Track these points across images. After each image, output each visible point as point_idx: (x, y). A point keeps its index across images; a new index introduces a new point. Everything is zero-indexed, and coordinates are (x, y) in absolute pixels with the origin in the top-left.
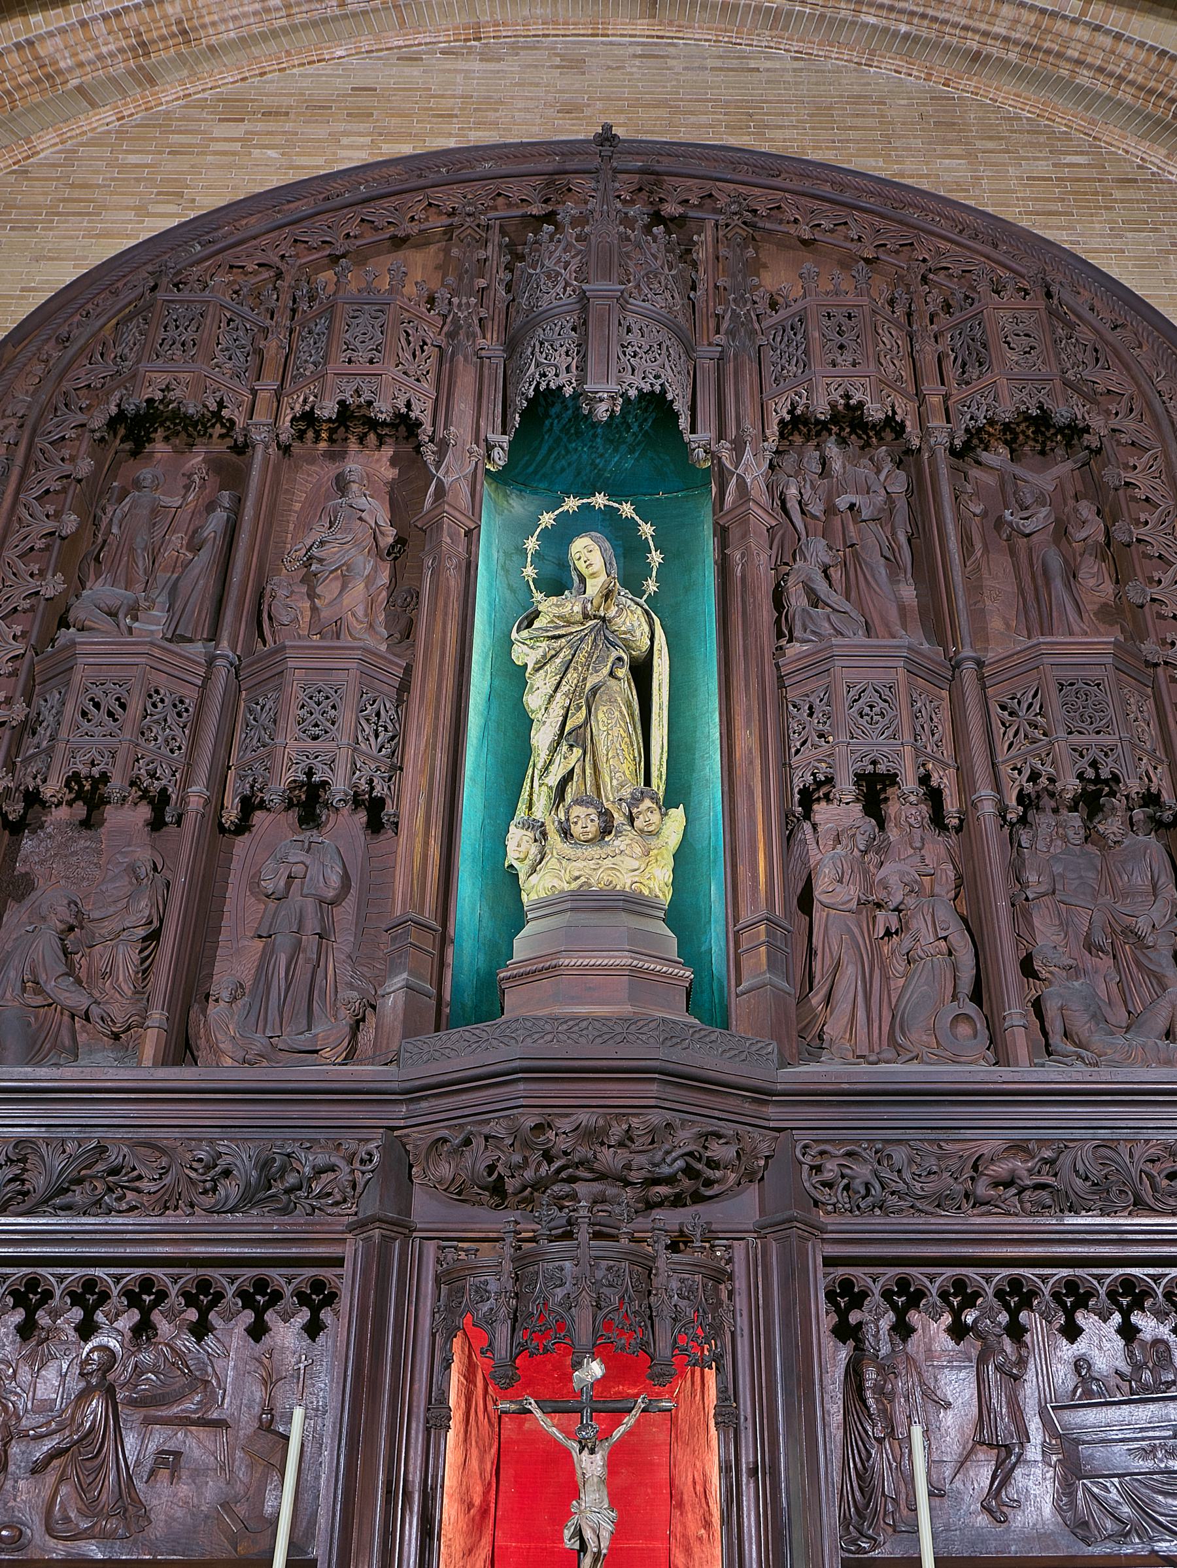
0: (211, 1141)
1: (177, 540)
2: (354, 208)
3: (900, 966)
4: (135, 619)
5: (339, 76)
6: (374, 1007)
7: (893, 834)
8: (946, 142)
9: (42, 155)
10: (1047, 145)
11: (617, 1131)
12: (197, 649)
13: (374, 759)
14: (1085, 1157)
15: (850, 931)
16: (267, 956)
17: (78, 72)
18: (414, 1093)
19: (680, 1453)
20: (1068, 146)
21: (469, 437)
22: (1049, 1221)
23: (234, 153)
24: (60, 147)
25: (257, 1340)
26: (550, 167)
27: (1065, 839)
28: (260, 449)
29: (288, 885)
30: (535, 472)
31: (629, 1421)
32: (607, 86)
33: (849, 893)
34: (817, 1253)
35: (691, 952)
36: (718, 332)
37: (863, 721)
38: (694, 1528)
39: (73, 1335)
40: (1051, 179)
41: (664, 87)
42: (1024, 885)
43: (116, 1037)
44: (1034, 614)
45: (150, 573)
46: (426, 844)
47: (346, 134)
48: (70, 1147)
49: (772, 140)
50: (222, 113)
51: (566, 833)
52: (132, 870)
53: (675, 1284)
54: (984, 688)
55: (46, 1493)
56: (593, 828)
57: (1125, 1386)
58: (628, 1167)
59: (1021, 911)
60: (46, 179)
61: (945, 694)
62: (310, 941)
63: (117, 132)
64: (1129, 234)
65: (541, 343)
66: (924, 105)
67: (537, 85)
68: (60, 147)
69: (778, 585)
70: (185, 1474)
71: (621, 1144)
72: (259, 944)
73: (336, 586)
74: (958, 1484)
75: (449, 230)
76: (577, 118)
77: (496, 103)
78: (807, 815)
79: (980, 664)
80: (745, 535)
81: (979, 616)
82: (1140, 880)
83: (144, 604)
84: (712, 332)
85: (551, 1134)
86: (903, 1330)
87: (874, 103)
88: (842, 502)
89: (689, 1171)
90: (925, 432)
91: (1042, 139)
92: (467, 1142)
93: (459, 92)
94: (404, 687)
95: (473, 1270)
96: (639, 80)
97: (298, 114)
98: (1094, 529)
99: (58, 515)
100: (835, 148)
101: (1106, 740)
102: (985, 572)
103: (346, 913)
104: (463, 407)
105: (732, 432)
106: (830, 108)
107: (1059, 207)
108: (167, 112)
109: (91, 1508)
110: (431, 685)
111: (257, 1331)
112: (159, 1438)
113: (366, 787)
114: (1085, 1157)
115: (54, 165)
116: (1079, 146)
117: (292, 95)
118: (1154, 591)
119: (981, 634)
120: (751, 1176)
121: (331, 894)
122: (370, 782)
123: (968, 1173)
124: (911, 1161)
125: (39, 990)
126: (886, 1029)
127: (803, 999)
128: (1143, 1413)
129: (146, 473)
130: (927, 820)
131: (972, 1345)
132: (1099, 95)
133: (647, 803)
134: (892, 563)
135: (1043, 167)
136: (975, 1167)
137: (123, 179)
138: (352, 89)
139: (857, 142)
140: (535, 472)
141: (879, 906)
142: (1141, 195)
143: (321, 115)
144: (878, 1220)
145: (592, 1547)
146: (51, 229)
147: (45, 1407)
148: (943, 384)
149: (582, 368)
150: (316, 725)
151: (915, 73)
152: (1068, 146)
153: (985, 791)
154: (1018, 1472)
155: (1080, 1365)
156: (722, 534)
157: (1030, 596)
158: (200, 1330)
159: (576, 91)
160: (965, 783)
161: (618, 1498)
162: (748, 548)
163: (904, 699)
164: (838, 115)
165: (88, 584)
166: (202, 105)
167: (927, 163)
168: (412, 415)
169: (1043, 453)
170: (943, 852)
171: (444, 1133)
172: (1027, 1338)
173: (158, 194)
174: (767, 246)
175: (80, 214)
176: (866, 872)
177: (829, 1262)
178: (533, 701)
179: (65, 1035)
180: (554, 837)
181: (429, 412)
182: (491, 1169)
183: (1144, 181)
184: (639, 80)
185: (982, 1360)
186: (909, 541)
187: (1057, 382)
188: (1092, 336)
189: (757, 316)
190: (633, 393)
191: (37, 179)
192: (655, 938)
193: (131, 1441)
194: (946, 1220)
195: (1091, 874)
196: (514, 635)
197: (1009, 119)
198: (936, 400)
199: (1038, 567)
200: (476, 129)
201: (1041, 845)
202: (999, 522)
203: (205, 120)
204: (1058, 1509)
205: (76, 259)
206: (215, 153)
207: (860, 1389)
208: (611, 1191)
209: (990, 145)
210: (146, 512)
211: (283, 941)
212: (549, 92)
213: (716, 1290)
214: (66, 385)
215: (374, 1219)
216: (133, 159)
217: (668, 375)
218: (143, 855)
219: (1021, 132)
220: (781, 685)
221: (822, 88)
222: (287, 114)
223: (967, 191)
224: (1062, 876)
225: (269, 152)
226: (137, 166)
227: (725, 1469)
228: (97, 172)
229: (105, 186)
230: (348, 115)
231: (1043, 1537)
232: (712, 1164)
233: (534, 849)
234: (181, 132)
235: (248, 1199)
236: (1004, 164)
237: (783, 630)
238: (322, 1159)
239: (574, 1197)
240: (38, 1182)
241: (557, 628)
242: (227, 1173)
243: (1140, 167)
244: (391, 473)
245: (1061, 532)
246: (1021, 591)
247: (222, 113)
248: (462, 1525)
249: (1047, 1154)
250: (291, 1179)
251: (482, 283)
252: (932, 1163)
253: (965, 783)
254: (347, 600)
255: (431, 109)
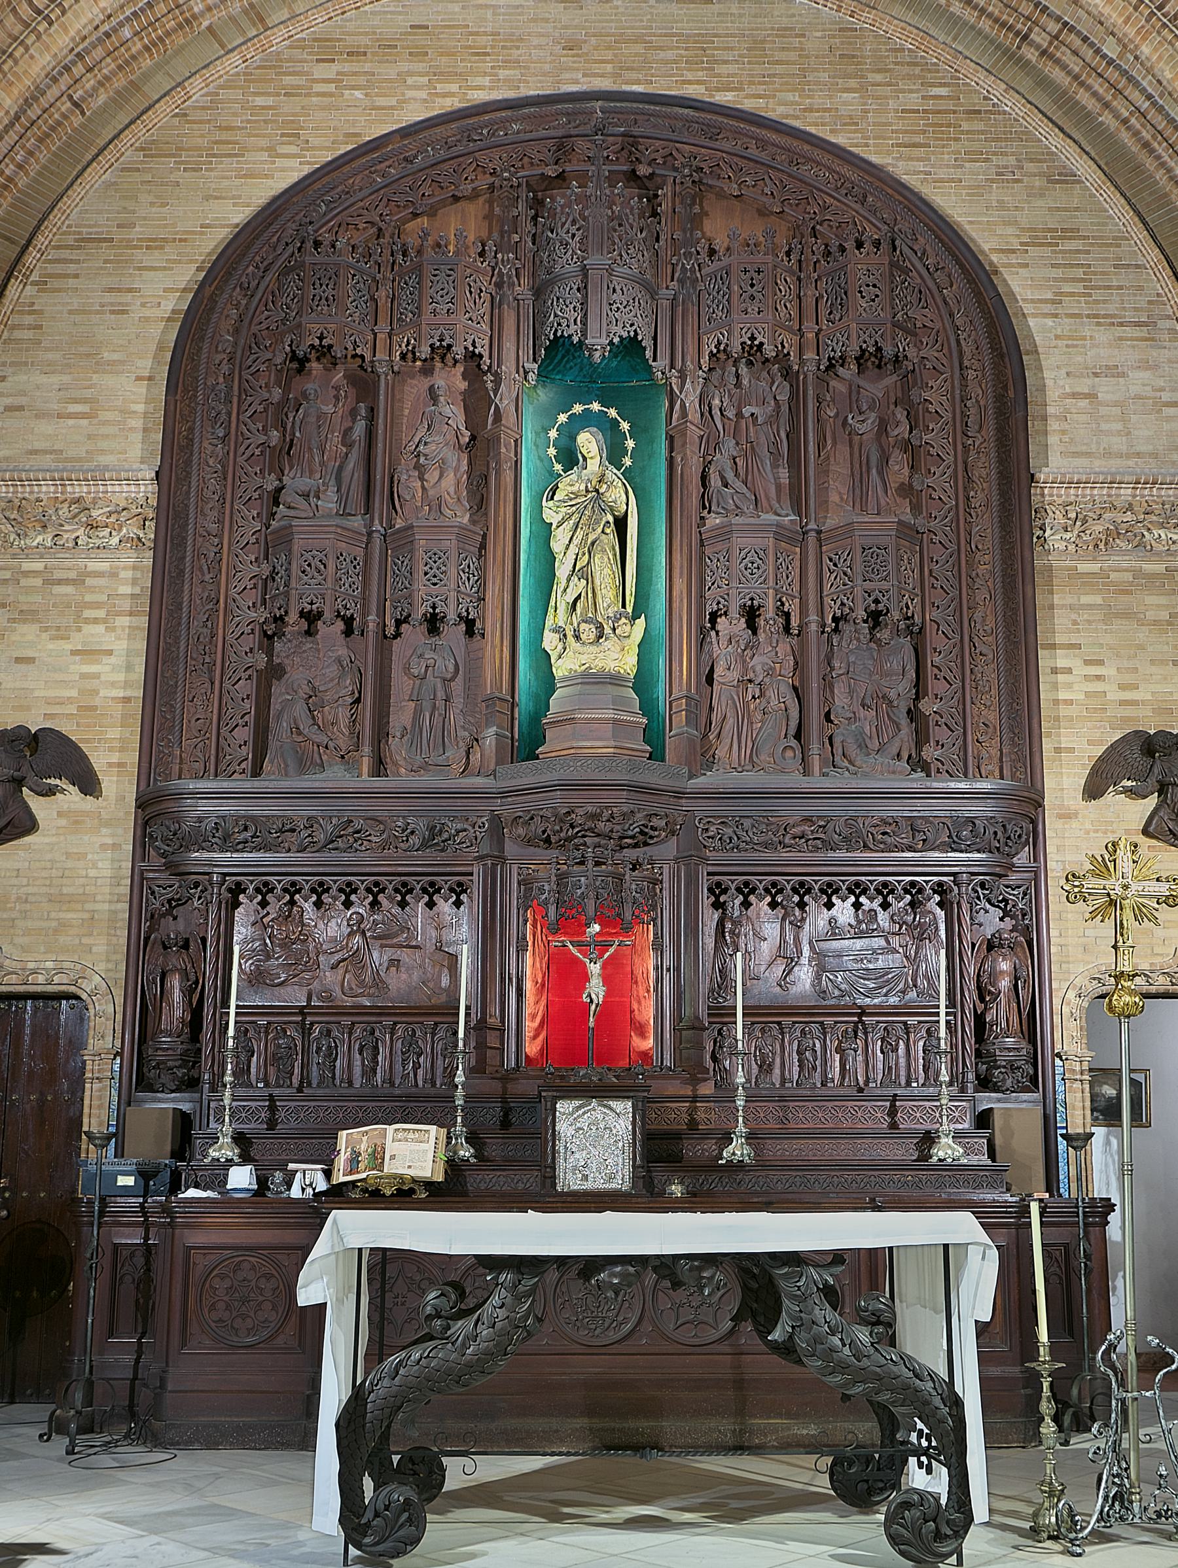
0: (404, 817)
1: (336, 437)
2: (427, 171)
3: (759, 716)
4: (318, 498)
5: (400, 13)
6: (477, 740)
7: (762, 636)
8: (847, 76)
9: (194, 98)
10: (920, 77)
11: (606, 814)
12: (357, 523)
13: (469, 595)
14: (840, 825)
15: (733, 698)
16: (418, 713)
17: (208, 15)
18: (504, 794)
19: (636, 960)
20: (936, 78)
21: (513, 370)
22: (820, 855)
23: (331, 95)
24: (206, 90)
25: (431, 909)
26: (560, 133)
27: (858, 640)
28: (383, 377)
29: (426, 671)
30: (553, 369)
31: (612, 950)
32: (600, 21)
33: (734, 675)
34: (703, 871)
35: (648, 707)
36: (672, 280)
37: (747, 573)
38: (642, 992)
39: (342, 907)
40: (918, 111)
41: (642, 21)
42: (832, 669)
43: (343, 757)
44: (858, 491)
45: (323, 464)
46: (502, 650)
47: (411, 74)
48: (334, 821)
49: (719, 75)
50: (318, 53)
51: (577, 637)
52: (339, 661)
53: (634, 887)
54: (821, 546)
55: (340, 978)
56: (592, 636)
57: (852, 931)
58: (612, 831)
59: (828, 683)
60: (201, 122)
61: (798, 550)
62: (440, 704)
63: (245, 74)
64: (967, 165)
65: (558, 299)
66: (834, 37)
67: (547, 20)
68: (206, 90)
69: (704, 470)
70: (403, 969)
71: (608, 820)
72: (412, 704)
73: (437, 474)
74: (767, 974)
75: (492, 187)
76: (578, 55)
77: (517, 40)
78: (713, 628)
79: (819, 532)
80: (685, 444)
81: (823, 490)
82: (896, 665)
83: (322, 488)
84: (669, 279)
85: (573, 816)
86: (746, 904)
87: (797, 36)
88: (747, 411)
89: (642, 833)
90: (802, 362)
91: (917, 70)
92: (532, 818)
93: (489, 29)
94: (483, 546)
95: (537, 880)
96: (623, 14)
97: (374, 54)
98: (903, 430)
99: (265, 430)
100: (765, 83)
101: (885, 585)
102: (832, 459)
103: (457, 686)
104: (509, 345)
105: (679, 364)
106: (763, 42)
107: (920, 139)
108: (278, 53)
109: (362, 984)
110: (499, 553)
111: (431, 905)
112: (389, 953)
113: (465, 614)
114: (840, 825)
115: (203, 108)
116: (943, 78)
117: (367, 34)
118: (929, 481)
119: (824, 504)
120: (673, 833)
121: (449, 676)
122: (467, 611)
123: (782, 832)
124: (753, 826)
125: (300, 733)
126: (748, 752)
127: (705, 736)
128: (859, 944)
129: (310, 387)
130: (781, 629)
131: (780, 912)
132: (966, 23)
133: (623, 620)
134: (775, 455)
135: (913, 100)
136: (785, 829)
137: (256, 121)
138: (412, 27)
139: (781, 76)
140: (553, 369)
141: (750, 681)
142: (980, 126)
143: (390, 54)
144: (735, 854)
145: (596, 1001)
146: (211, 170)
147: (334, 940)
148: (817, 324)
149: (584, 323)
150: (435, 576)
151: (829, 5)
152: (936, 78)
153: (813, 617)
154: (796, 969)
155: (832, 921)
156: (671, 439)
157: (857, 479)
158: (403, 904)
159: (576, 27)
160: (803, 612)
161: (607, 979)
162: (685, 454)
163: (771, 558)
164: (770, 49)
165: (286, 472)
166: (300, 45)
167: (831, 97)
168: (477, 351)
169: (879, 367)
170: (789, 648)
171: (520, 814)
172: (807, 908)
173: (283, 135)
174: (710, 195)
175: (230, 155)
176: (745, 661)
177: (709, 874)
178: (557, 546)
179: (316, 756)
180: (571, 639)
181: (487, 347)
182: (544, 832)
183: (986, 112)
184: (623, 14)
185: (783, 919)
186: (787, 436)
187: (889, 325)
188: (919, 281)
189: (699, 265)
190: (616, 340)
191: (194, 122)
192: (626, 700)
193: (375, 955)
194: (769, 855)
195: (871, 662)
196: (544, 503)
197: (897, 50)
198: (811, 335)
199: (864, 458)
200: (505, 68)
201: (844, 644)
202: (845, 423)
203: (305, 61)
204: (813, 986)
205: (233, 197)
206: (319, 94)
207: (723, 932)
208: (603, 842)
209: (878, 77)
210: (314, 420)
211: (427, 705)
212: (555, 27)
213: (654, 888)
214: (254, 329)
215: (487, 856)
216: (260, 101)
217: (639, 321)
218: (343, 652)
219: (902, 64)
220: (702, 545)
221: (759, 20)
222: (365, 54)
223: (857, 124)
224: (854, 663)
225: (356, 93)
226: (263, 108)
227: (656, 968)
228: (235, 114)
229: (243, 128)
230: (411, 54)
231: (803, 996)
232: (653, 829)
233: (560, 646)
234: (290, 74)
235: (424, 845)
236: (886, 98)
237: (705, 504)
238: (459, 826)
239: (585, 844)
240: (321, 837)
241: (571, 499)
242: (412, 833)
243: (985, 98)
244: (463, 385)
245: (883, 427)
246: (852, 474)
247: (318, 53)
248: (534, 991)
249: (822, 823)
250: (445, 836)
251: (516, 237)
252: (763, 828)
253: (803, 612)
254: (444, 483)
255: (470, 47)
